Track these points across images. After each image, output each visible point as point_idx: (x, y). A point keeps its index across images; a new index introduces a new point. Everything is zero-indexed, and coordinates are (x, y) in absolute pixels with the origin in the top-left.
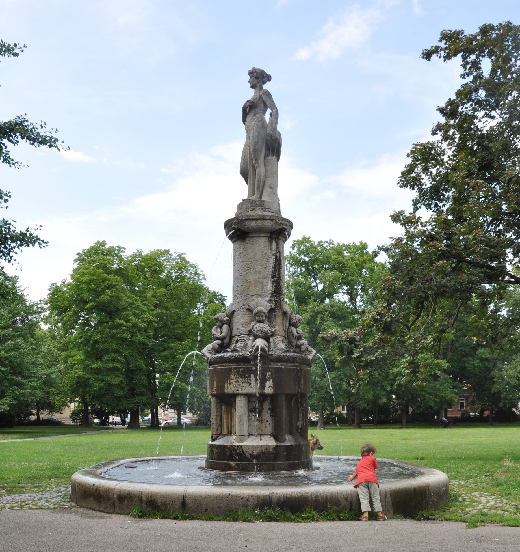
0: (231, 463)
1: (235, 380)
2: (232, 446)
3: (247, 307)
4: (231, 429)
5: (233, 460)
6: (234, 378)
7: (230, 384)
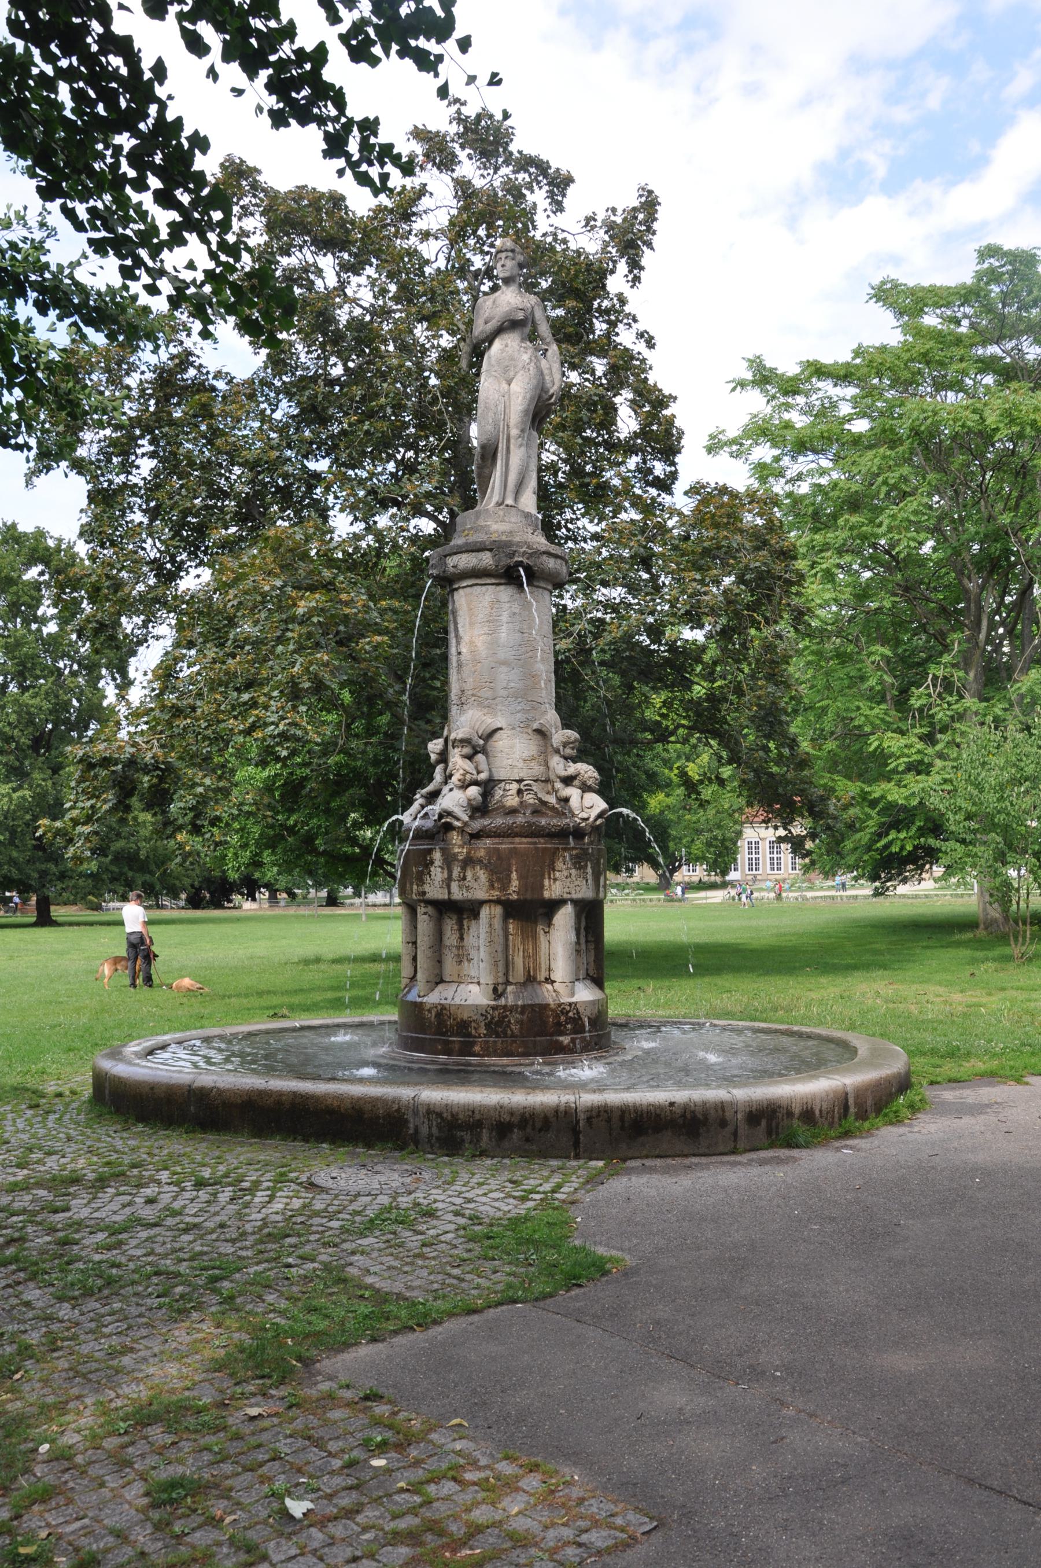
0: (561, 1038)
1: (566, 873)
2: (560, 1005)
3: (535, 726)
4: (535, 970)
5: (562, 1034)
6: (563, 867)
7: (555, 880)
